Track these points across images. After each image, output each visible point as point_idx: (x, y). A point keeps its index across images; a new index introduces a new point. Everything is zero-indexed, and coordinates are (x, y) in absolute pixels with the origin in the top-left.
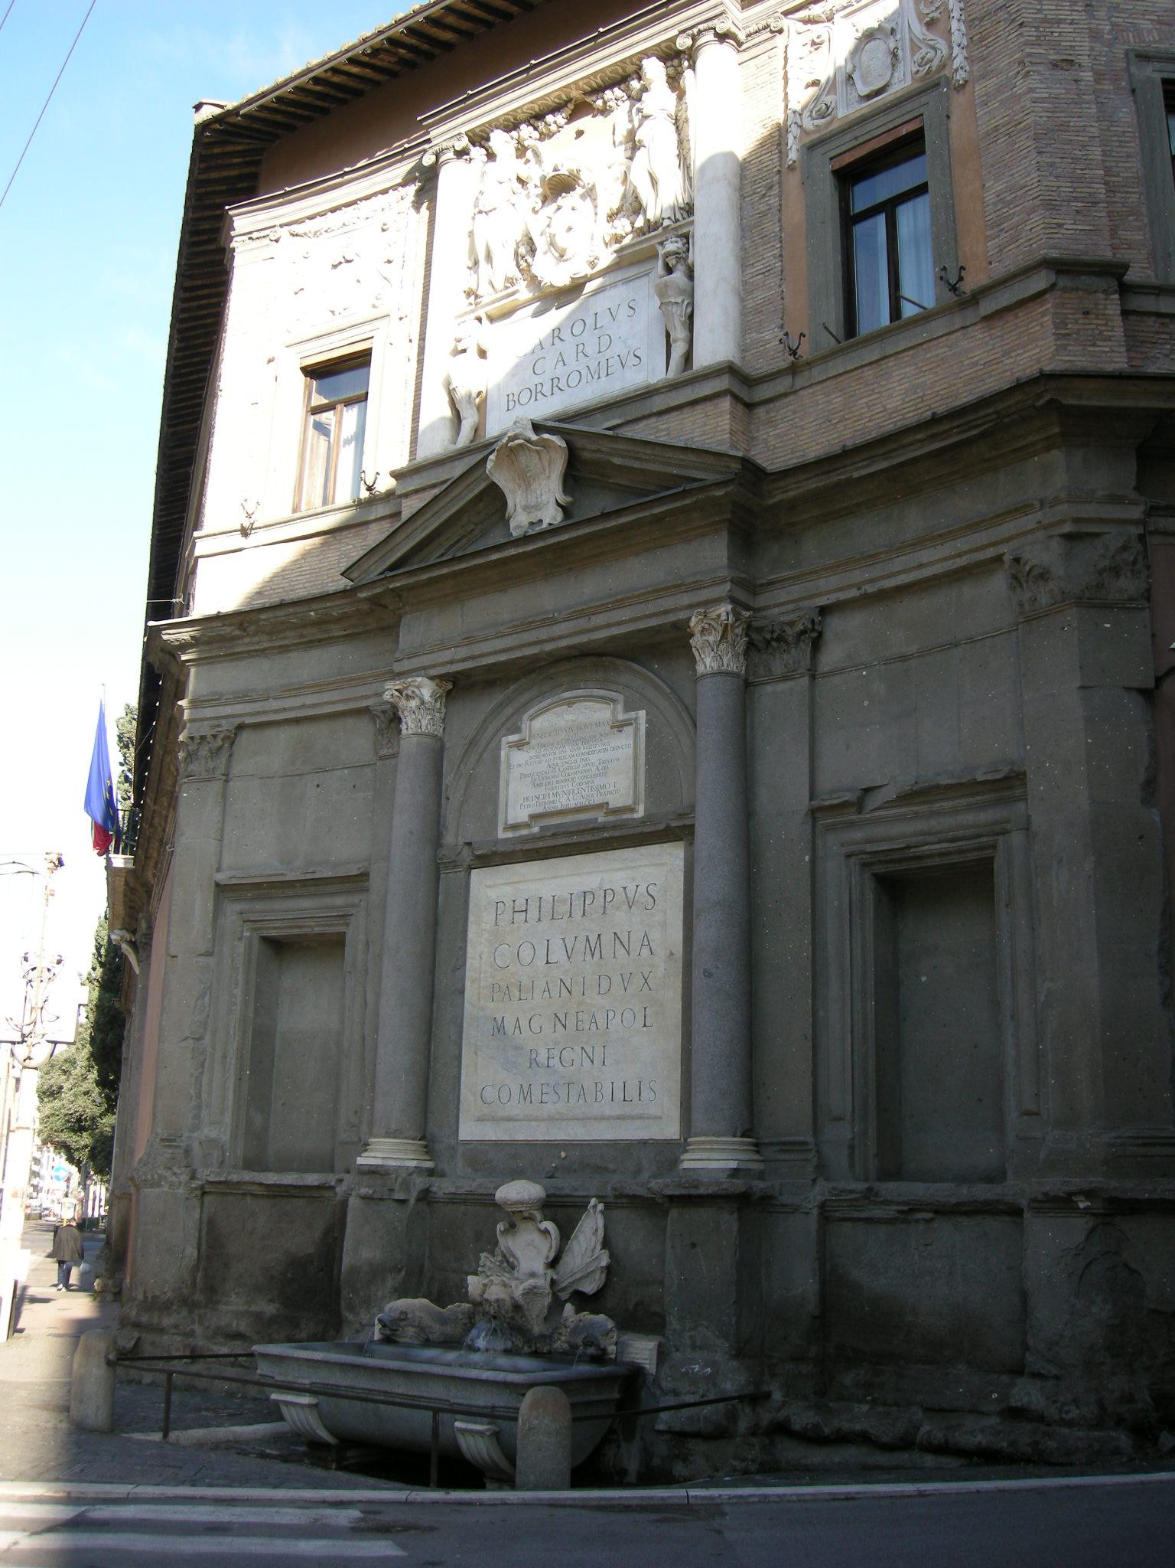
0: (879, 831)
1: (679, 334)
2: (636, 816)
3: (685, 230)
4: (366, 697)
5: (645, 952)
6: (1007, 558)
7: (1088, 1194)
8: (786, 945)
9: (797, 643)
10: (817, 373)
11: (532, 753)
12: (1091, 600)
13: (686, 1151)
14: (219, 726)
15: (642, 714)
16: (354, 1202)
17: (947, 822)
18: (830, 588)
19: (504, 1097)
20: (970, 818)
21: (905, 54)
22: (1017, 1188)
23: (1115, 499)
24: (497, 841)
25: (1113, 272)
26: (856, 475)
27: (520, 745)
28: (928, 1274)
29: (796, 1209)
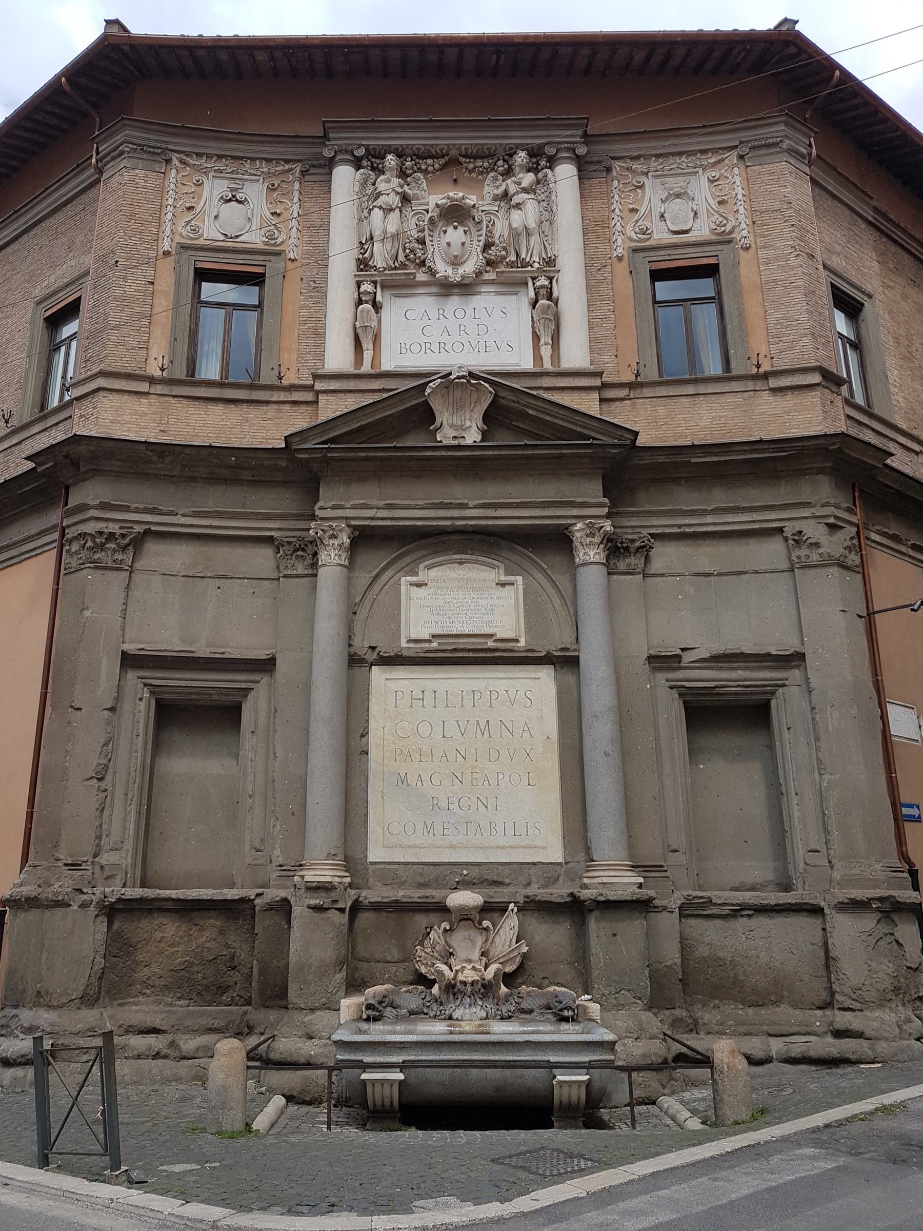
3: (552, 275)
5: (526, 735)
7: (881, 899)
9: (636, 553)
10: (647, 392)
11: (431, 591)
14: (132, 528)
15: (520, 579)
18: (661, 524)
26: (693, 460)
27: (419, 585)
29: (664, 908)
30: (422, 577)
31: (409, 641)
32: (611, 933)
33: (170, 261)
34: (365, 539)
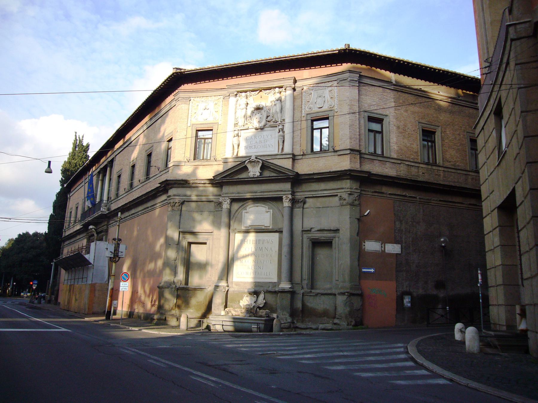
0: (313, 235)
1: (281, 144)
6: (339, 196)
7: (347, 292)
8: (297, 252)
10: (307, 157)
12: (352, 205)
17: (326, 235)
18: (308, 194)
20: (329, 235)
21: (326, 101)
22: (333, 291)
23: (356, 189)
25: (359, 151)
27: (247, 213)
28: (319, 304)
29: (298, 294)
33: (190, 128)
34: (234, 200)
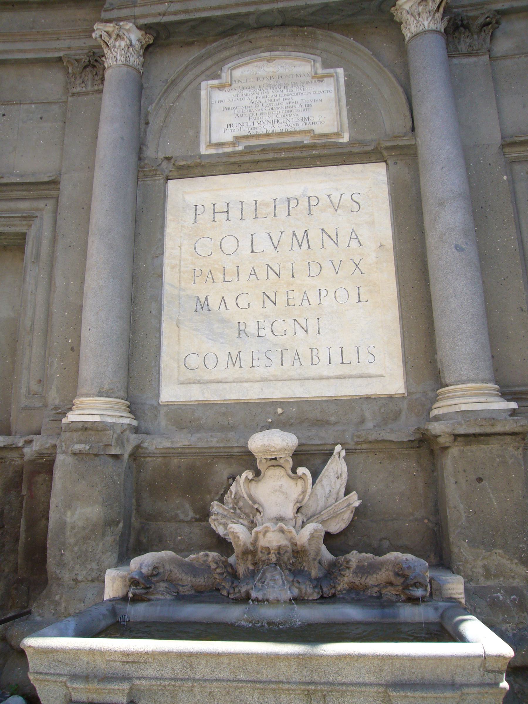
2: (341, 141)
4: (59, 50)
5: (354, 244)
11: (235, 93)
13: (437, 401)
15: (340, 71)
16: (62, 460)
19: (210, 363)
24: (201, 156)
27: (221, 87)
30: (225, 75)
31: (210, 145)
32: (475, 477)
